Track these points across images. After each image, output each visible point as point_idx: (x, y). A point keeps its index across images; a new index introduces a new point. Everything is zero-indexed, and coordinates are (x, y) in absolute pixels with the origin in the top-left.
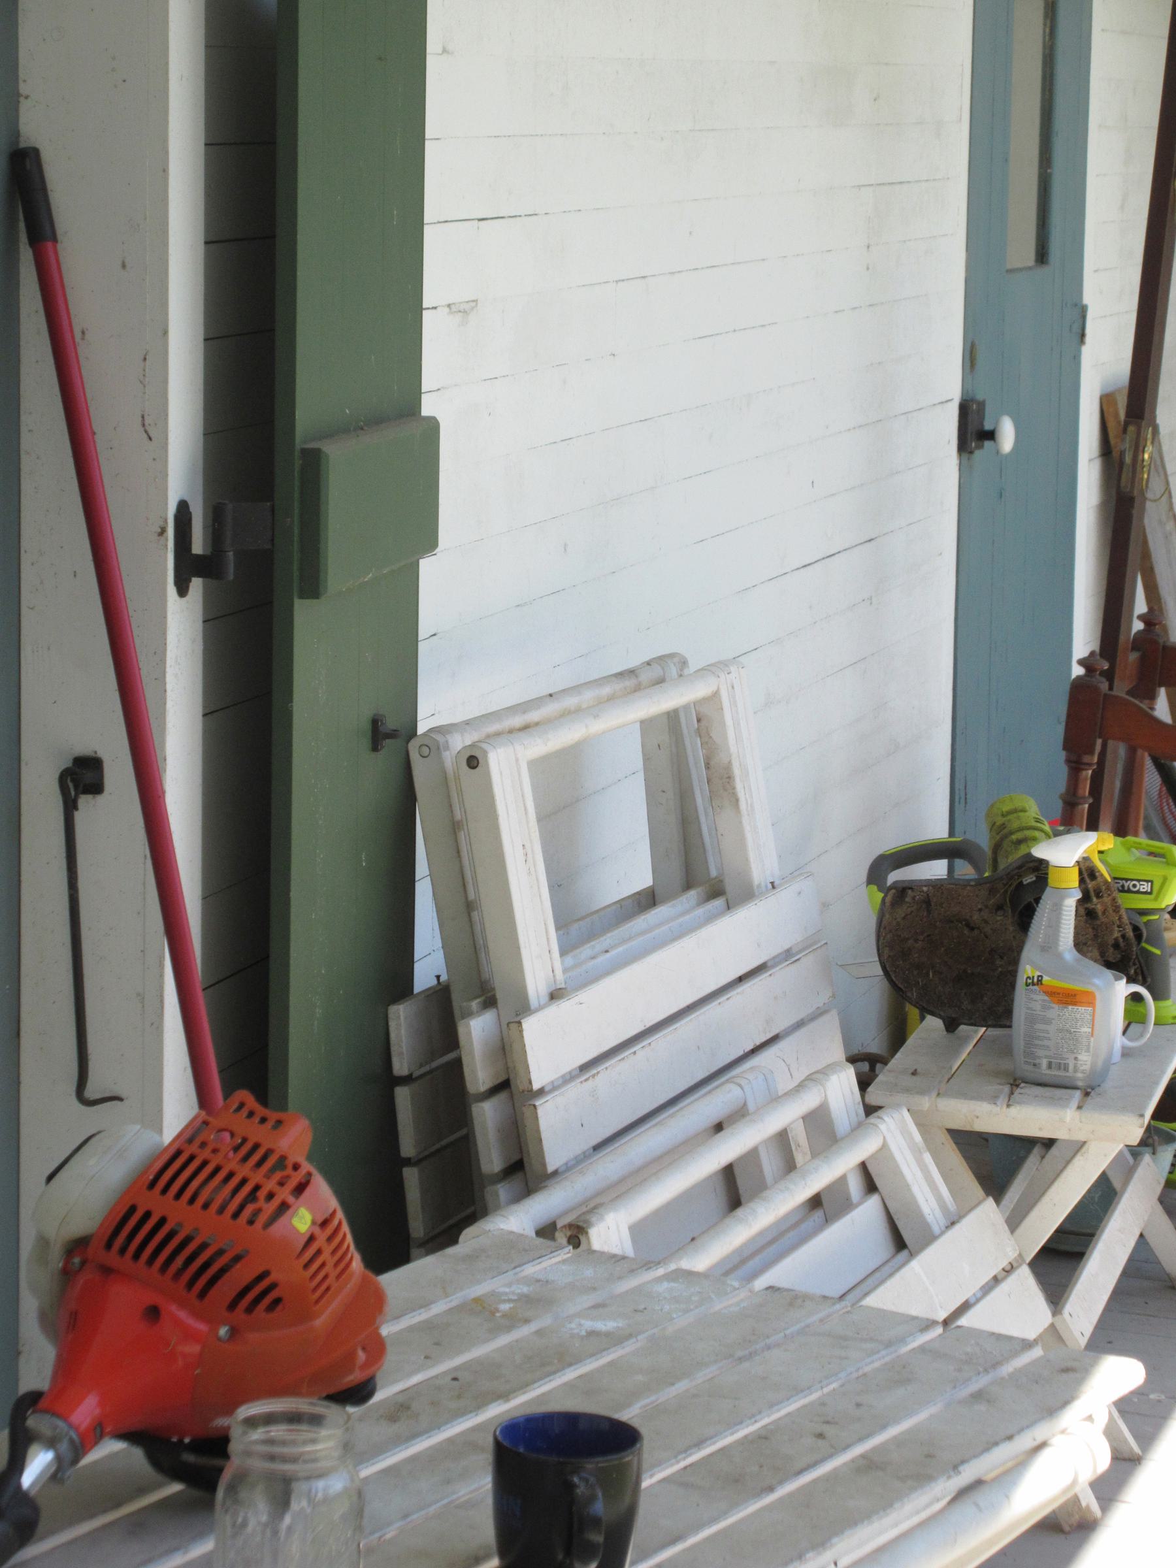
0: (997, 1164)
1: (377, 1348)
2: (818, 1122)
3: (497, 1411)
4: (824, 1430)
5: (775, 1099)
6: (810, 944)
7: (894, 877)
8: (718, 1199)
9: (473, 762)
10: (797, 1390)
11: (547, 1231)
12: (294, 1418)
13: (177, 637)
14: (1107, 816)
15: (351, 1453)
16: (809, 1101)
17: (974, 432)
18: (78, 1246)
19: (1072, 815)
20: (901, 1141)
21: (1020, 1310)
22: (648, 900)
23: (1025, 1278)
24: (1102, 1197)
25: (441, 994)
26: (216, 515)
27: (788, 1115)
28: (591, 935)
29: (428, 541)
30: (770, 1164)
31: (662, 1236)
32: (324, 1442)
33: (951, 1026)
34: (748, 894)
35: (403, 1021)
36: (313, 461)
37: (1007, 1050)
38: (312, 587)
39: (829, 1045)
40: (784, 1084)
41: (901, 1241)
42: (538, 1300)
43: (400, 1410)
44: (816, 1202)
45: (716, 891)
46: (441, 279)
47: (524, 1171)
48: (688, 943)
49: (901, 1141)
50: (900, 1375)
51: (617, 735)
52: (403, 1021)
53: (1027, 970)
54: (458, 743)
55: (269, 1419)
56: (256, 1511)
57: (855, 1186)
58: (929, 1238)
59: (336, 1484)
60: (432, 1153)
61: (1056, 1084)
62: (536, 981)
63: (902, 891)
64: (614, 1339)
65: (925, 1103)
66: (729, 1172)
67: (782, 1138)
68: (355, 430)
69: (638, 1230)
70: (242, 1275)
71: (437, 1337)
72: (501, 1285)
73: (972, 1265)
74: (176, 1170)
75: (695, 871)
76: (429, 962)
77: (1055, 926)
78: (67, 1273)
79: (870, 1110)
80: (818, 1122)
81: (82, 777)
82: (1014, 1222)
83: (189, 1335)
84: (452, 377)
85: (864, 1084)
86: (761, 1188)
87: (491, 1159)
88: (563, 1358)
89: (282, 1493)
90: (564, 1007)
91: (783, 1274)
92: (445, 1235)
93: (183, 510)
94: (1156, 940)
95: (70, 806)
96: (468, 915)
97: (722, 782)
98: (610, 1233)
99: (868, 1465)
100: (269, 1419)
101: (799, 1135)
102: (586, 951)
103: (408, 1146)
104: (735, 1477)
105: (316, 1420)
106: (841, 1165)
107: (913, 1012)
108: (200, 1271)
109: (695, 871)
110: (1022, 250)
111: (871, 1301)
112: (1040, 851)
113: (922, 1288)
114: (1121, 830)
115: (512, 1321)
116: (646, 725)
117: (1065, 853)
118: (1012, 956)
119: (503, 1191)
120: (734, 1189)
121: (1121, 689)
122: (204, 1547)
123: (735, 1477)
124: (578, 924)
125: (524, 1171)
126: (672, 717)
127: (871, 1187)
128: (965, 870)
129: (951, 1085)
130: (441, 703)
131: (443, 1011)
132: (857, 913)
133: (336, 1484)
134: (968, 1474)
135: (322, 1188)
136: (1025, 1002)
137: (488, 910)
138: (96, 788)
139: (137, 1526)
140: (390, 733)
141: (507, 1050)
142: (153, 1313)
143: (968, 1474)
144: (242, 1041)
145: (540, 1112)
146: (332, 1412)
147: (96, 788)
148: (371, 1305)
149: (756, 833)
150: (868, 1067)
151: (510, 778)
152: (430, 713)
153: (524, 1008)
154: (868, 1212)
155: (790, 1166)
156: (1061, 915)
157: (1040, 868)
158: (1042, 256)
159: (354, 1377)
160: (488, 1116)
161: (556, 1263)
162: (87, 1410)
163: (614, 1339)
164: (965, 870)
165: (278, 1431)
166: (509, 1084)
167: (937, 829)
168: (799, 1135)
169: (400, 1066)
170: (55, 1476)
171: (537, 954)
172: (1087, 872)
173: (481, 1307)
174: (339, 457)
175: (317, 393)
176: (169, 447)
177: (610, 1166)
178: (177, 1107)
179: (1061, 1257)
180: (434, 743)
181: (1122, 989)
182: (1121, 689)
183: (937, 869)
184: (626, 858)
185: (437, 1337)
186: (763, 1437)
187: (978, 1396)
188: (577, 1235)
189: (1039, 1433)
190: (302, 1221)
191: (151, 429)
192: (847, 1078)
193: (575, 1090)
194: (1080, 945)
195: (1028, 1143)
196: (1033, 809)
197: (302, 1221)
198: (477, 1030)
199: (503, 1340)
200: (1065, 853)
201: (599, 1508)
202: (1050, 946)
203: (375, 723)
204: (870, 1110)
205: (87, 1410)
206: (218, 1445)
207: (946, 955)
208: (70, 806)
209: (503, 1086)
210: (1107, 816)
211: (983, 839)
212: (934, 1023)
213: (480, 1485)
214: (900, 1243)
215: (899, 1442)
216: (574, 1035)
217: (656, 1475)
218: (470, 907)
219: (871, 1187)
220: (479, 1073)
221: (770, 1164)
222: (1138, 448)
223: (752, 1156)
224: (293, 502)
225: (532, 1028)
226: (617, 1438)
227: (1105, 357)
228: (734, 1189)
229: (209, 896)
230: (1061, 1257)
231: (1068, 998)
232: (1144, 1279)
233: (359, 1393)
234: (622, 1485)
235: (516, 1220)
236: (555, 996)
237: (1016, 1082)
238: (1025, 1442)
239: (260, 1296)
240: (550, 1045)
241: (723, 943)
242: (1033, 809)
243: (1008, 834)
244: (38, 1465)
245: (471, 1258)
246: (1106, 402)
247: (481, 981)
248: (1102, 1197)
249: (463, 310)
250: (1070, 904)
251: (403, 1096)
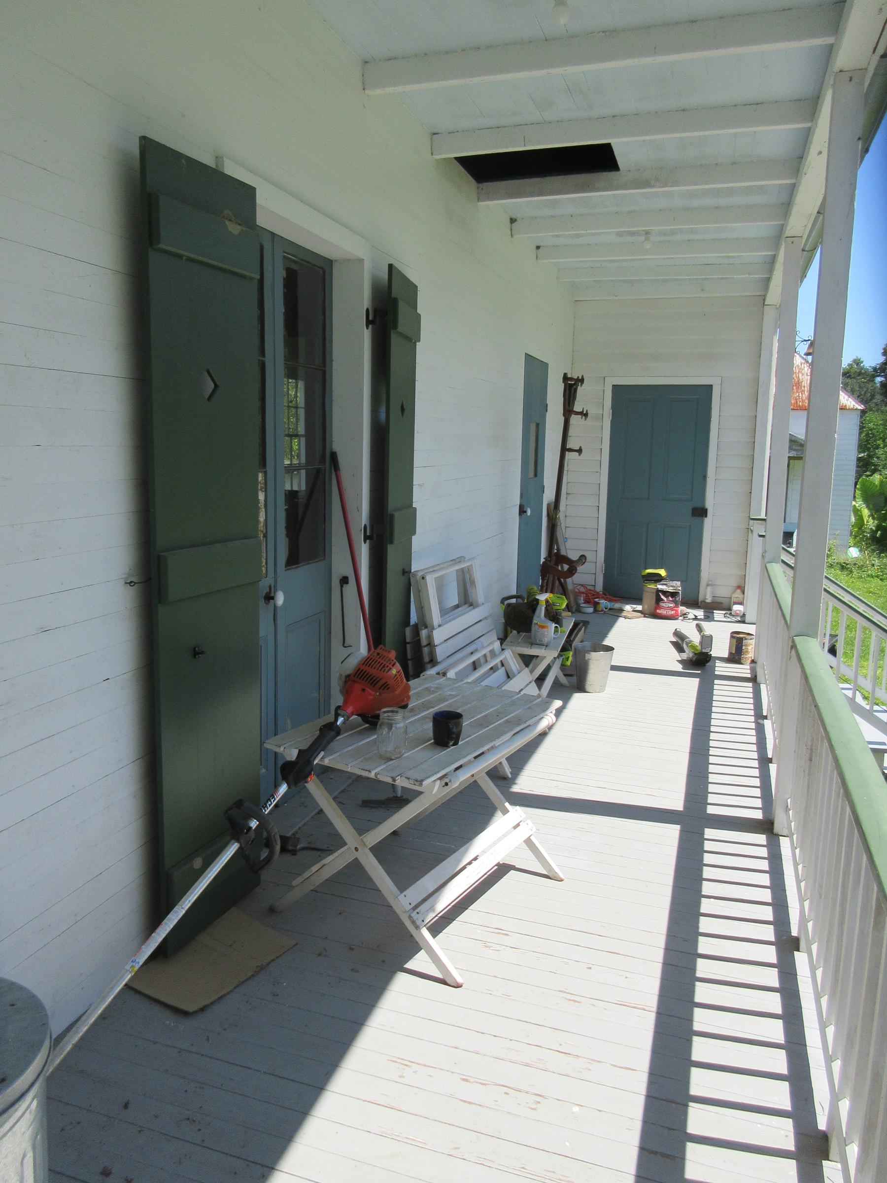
0: (527, 660)
1: (409, 698)
2: (492, 652)
3: (436, 709)
4: (498, 715)
5: (483, 647)
6: (490, 616)
7: (506, 602)
8: (471, 668)
9: (423, 578)
10: (492, 707)
11: (438, 674)
12: (392, 711)
13: (364, 552)
14: (549, 590)
15: (404, 718)
16: (490, 648)
17: (522, 511)
18: (348, 676)
19: (543, 590)
20: (509, 656)
21: (533, 690)
22: (457, 607)
23: (534, 684)
24: (549, 667)
25: (416, 625)
26: (372, 527)
27: (486, 651)
28: (446, 614)
29: (414, 533)
30: (482, 661)
31: (461, 675)
32: (399, 717)
33: (518, 633)
34: (478, 606)
35: (408, 631)
36: (392, 516)
37: (530, 637)
38: (392, 542)
39: (494, 636)
40: (485, 644)
41: (509, 676)
42: (438, 688)
43: (412, 710)
44: (492, 668)
45: (471, 605)
46: (416, 480)
47: (433, 662)
48: (466, 616)
49: (509, 656)
50: (513, 703)
51: (451, 572)
52: (408, 631)
53: (535, 621)
54: (420, 574)
55: (388, 712)
56: (385, 731)
57: (500, 665)
58: (515, 676)
59: (401, 725)
60: (416, 658)
61: (540, 645)
62: (436, 623)
63: (509, 605)
64: (455, 696)
65: (514, 648)
66: (474, 663)
67: (485, 656)
68: (861, 422)
69: (456, 674)
70: (381, 683)
71: (419, 695)
72: (431, 685)
73: (523, 682)
74: (367, 662)
75: (467, 601)
76: (414, 619)
77: (540, 612)
78: (346, 682)
79: (503, 650)
80: (492, 652)
81: (344, 580)
82: (531, 672)
83: (370, 694)
84: (419, 500)
85: (501, 644)
86: (480, 666)
87: (426, 659)
88: (445, 700)
89: (390, 727)
90: (442, 628)
91: (484, 683)
92: (417, 675)
93: (365, 526)
94: (560, 615)
95: (342, 587)
96: (421, 610)
97: (473, 583)
98: (451, 674)
99: (507, 722)
100: (388, 712)
101: (488, 655)
102: (447, 616)
103: (409, 657)
104: (484, 722)
105: (397, 712)
106: (497, 661)
107: (509, 629)
108: (373, 681)
109: (467, 601)
110: (531, 474)
111: (503, 689)
112: (537, 597)
113: (514, 685)
114: (552, 592)
115: (433, 692)
116: (457, 571)
117: (543, 597)
118: (531, 619)
119: (429, 666)
120: (475, 666)
121: (552, 564)
122: (375, 737)
123: (484, 722)
124: (444, 612)
125: (433, 662)
126: (462, 569)
127: (503, 665)
128: (520, 601)
129: (519, 645)
130: (416, 566)
131: (416, 629)
132: (500, 610)
133: (401, 725)
134: (528, 724)
135: (398, 664)
136: (534, 628)
137: (426, 608)
138: (347, 583)
139: (360, 733)
140: (406, 572)
141: (430, 637)
142: (363, 690)
143: (528, 724)
144: (376, 636)
145: (621, 624)
146: (400, 710)
147: (347, 583)
148: (408, 688)
149: (480, 593)
150: (502, 640)
151: (430, 580)
152: (414, 568)
153: (433, 628)
154: (502, 671)
155: (486, 661)
156: (541, 610)
157: (537, 600)
158: (536, 475)
159: (403, 704)
160: (426, 650)
161: (442, 680)
162: (350, 709)
163: (455, 696)
164: (520, 601)
165: (390, 714)
166: (430, 644)
167: (514, 593)
168: (488, 655)
169: (408, 640)
170: (344, 723)
171: (436, 617)
172: (547, 601)
173: (427, 689)
174: (397, 515)
175: (393, 502)
176: (362, 514)
177: (451, 660)
178: (363, 649)
179: (540, 680)
180: (415, 574)
181: (554, 625)
182: (552, 564)
183: (514, 601)
184: (453, 599)
185: (419, 695)
186: (486, 716)
187: (529, 708)
188: (444, 674)
189: (542, 715)
190: (394, 671)
191: (359, 509)
192: (498, 643)
193: (443, 645)
194: (545, 616)
195: (533, 656)
196: (535, 588)
197: (394, 671)
198: (424, 633)
199: (432, 696)
200: (543, 597)
201: (454, 730)
202: (539, 617)
203: (403, 570)
204: (503, 650)
205: (350, 709)
206: (377, 717)
207: (518, 619)
208: (342, 587)
209: (429, 644)
210: (549, 590)
211: (525, 595)
212: (515, 632)
213: (430, 725)
214: (508, 677)
215: (513, 717)
216: (443, 634)
217: (465, 723)
218: (422, 608)
219: (503, 665)
220: (424, 642)
221: (482, 661)
222: (556, 514)
223: (479, 659)
224: (387, 525)
225: (435, 632)
226: (458, 716)
227: (549, 495)
228: (475, 666)
229: (369, 605)
230: (540, 680)
231: (543, 627)
232: (557, 684)
233: (405, 707)
234: (459, 725)
235: (431, 672)
236: (439, 626)
237: (532, 644)
238: (538, 717)
239: (385, 687)
240: (438, 636)
241: (473, 615)
242: (535, 588)
243: (530, 594)
244: (340, 720)
245: (425, 679)
246: (548, 505)
247: (424, 623)
248: (549, 667)
249: (420, 485)
250: (543, 608)
251: (408, 646)
